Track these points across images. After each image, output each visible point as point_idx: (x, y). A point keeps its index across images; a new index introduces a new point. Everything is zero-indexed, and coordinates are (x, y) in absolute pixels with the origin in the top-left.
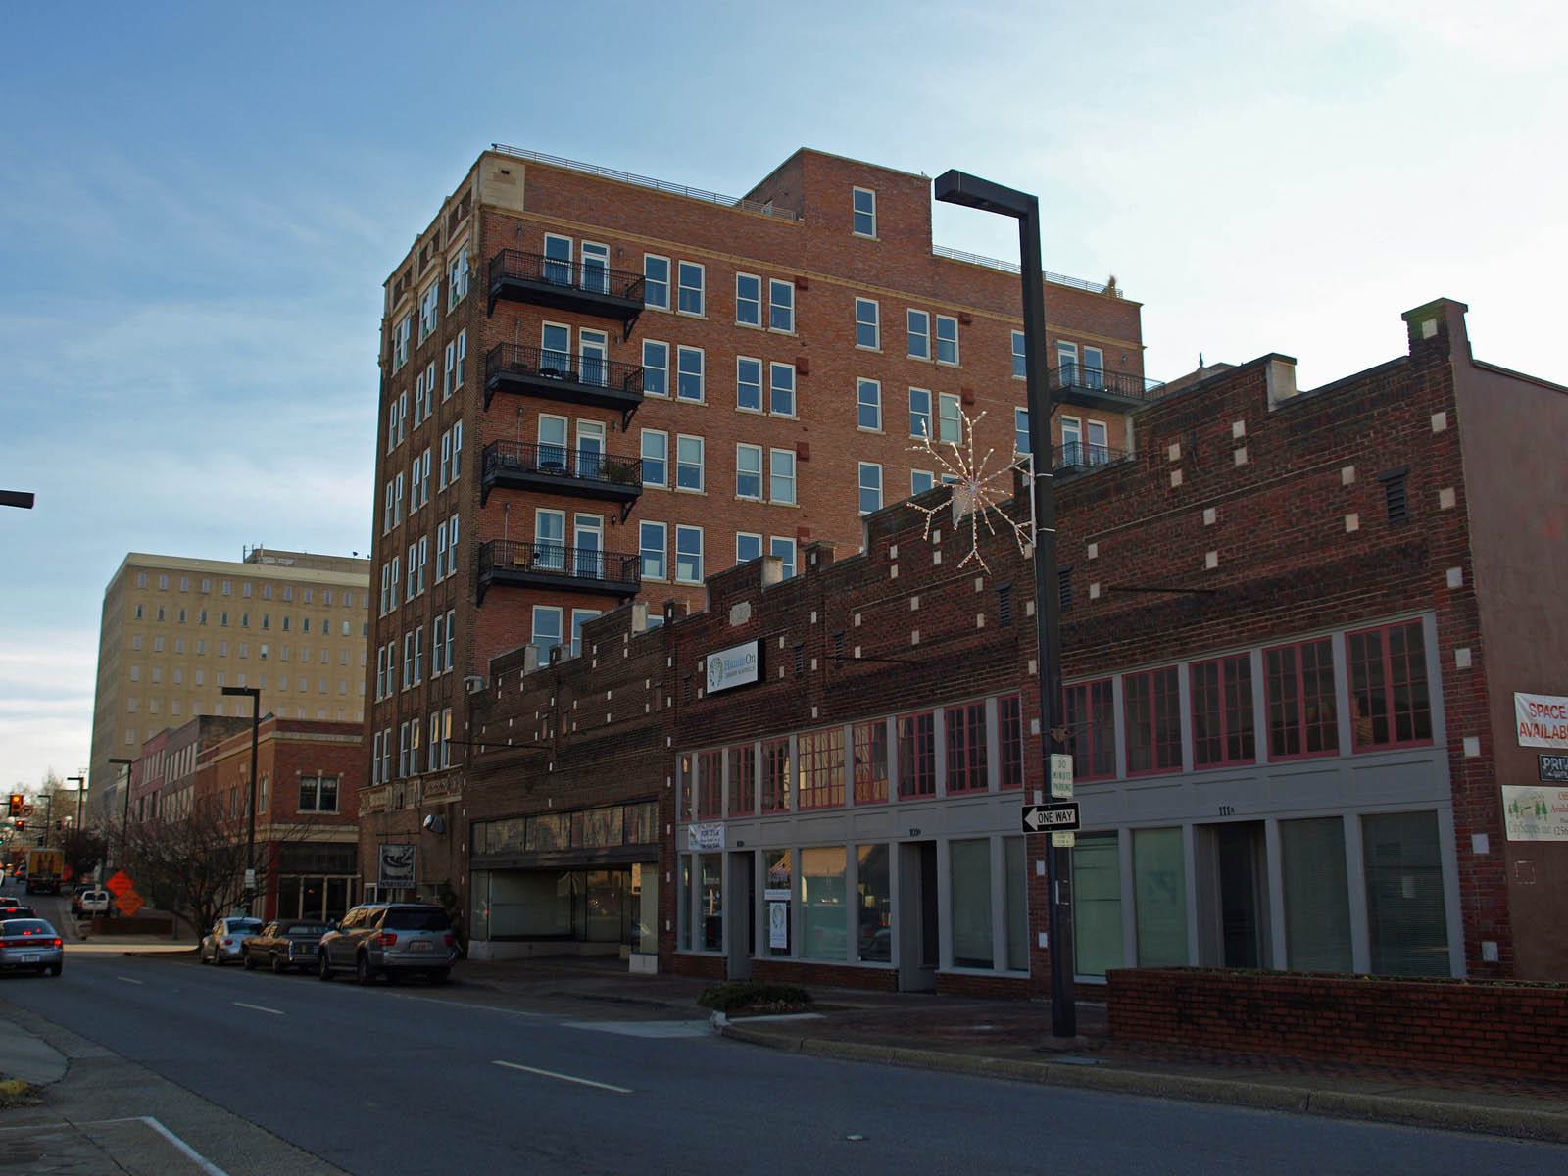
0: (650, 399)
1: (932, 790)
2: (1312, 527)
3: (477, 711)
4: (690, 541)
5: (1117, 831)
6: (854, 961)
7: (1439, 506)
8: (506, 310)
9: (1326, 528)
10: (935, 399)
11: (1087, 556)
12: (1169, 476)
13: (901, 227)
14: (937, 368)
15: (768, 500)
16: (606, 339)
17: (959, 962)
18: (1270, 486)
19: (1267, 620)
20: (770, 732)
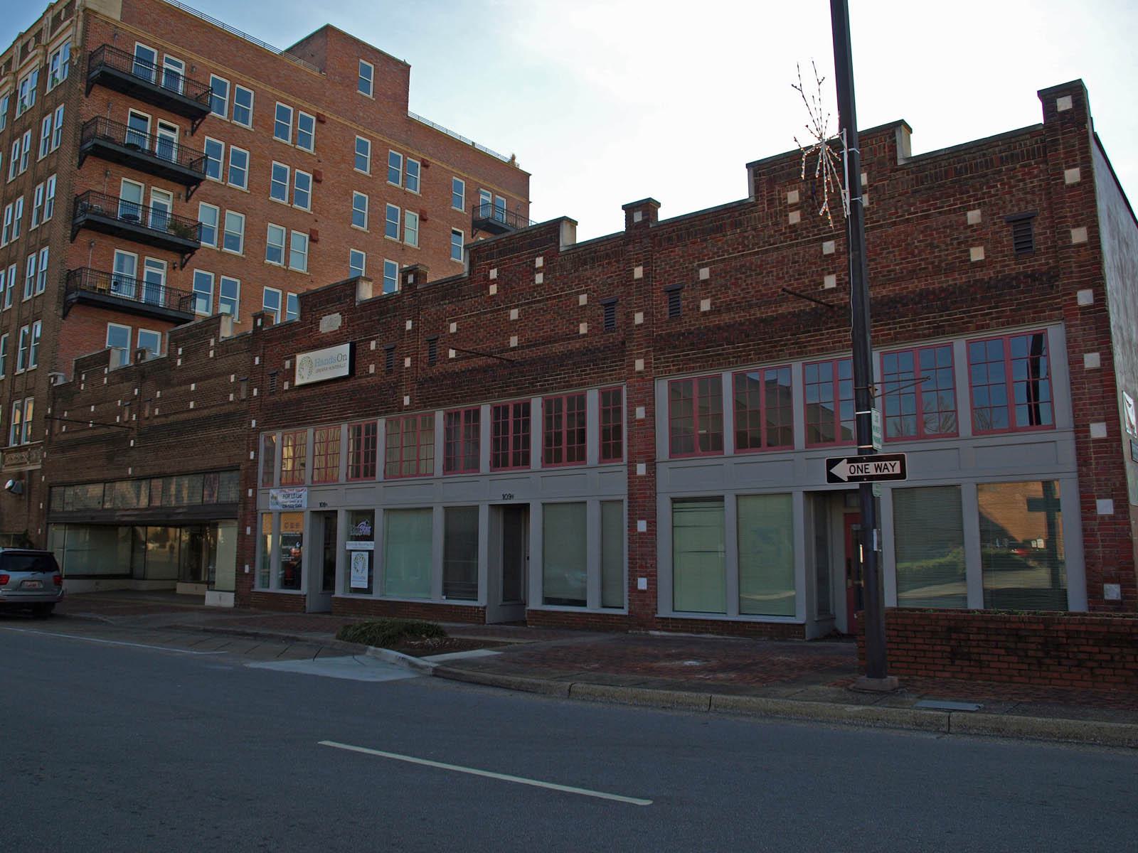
0: (209, 181)
1: (373, 474)
2: (935, 257)
3: (60, 400)
4: (230, 289)
5: (723, 497)
6: (438, 598)
7: (1070, 242)
8: (100, 94)
9: (950, 258)
10: (403, 214)
11: (699, 278)
12: (787, 216)
13: (390, 93)
14: (406, 193)
15: (288, 266)
16: (177, 130)
17: (548, 600)
18: (894, 224)
19: (890, 329)
20: (358, 416)
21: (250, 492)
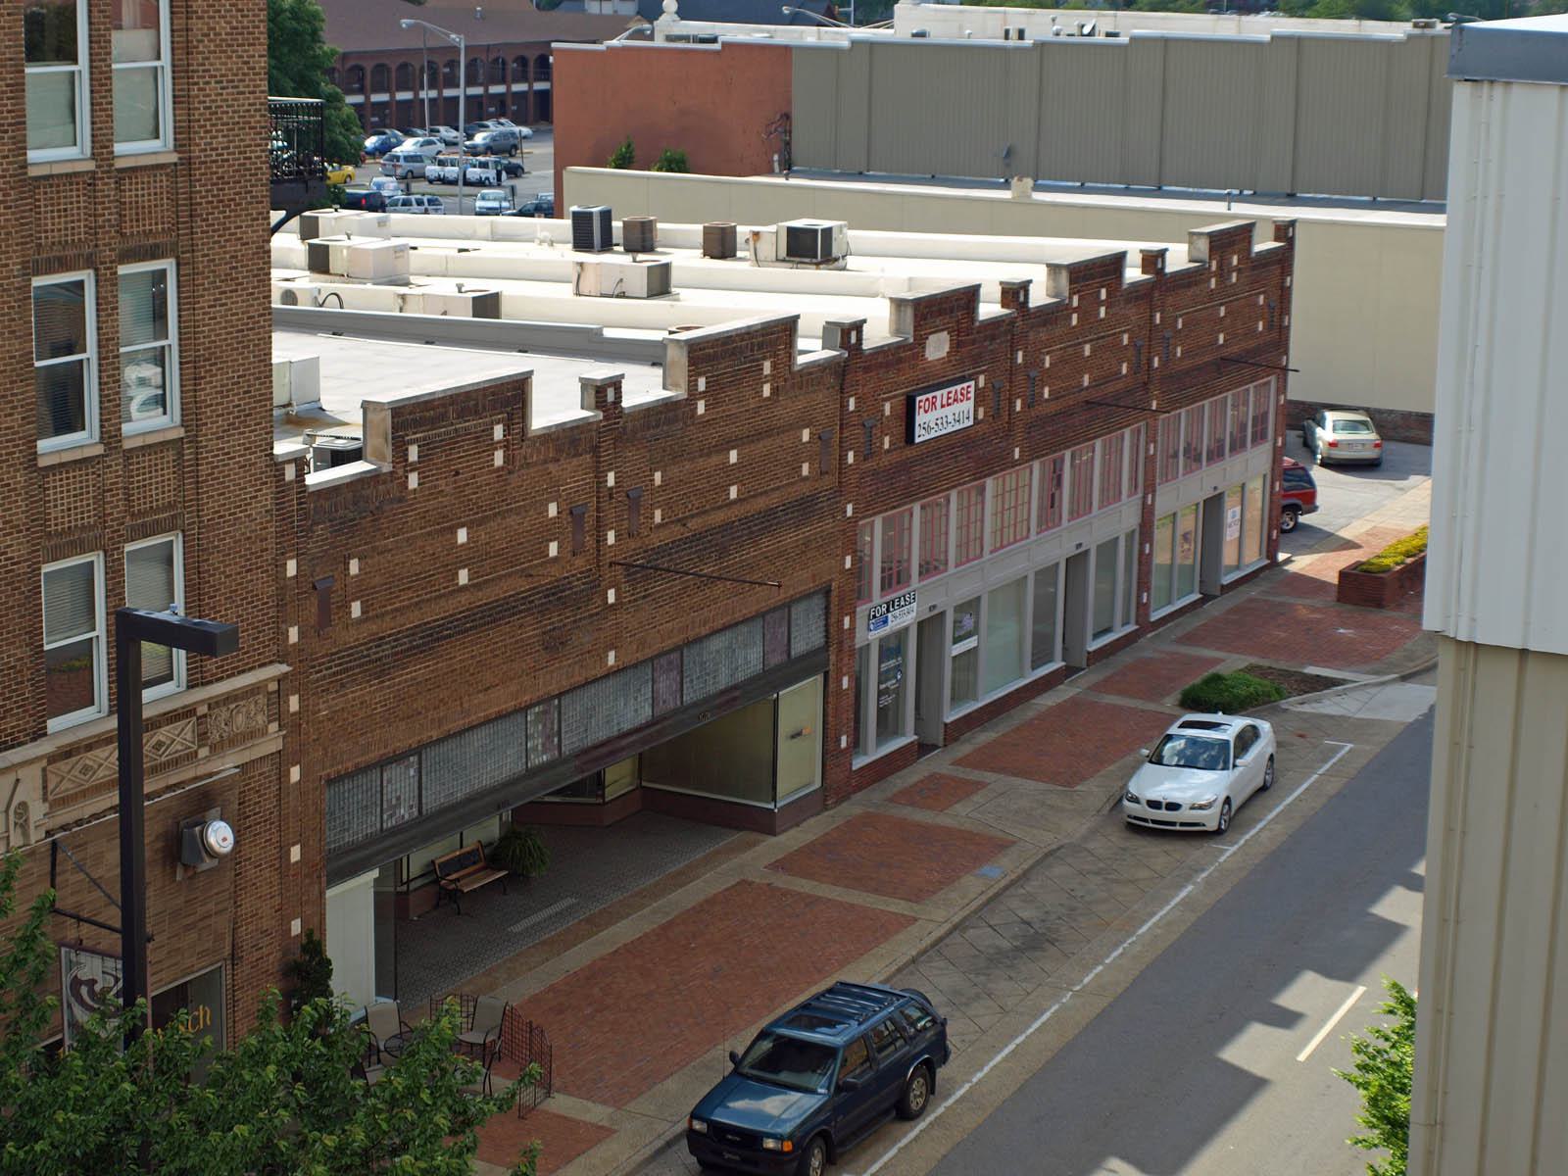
21: (847, 620)
